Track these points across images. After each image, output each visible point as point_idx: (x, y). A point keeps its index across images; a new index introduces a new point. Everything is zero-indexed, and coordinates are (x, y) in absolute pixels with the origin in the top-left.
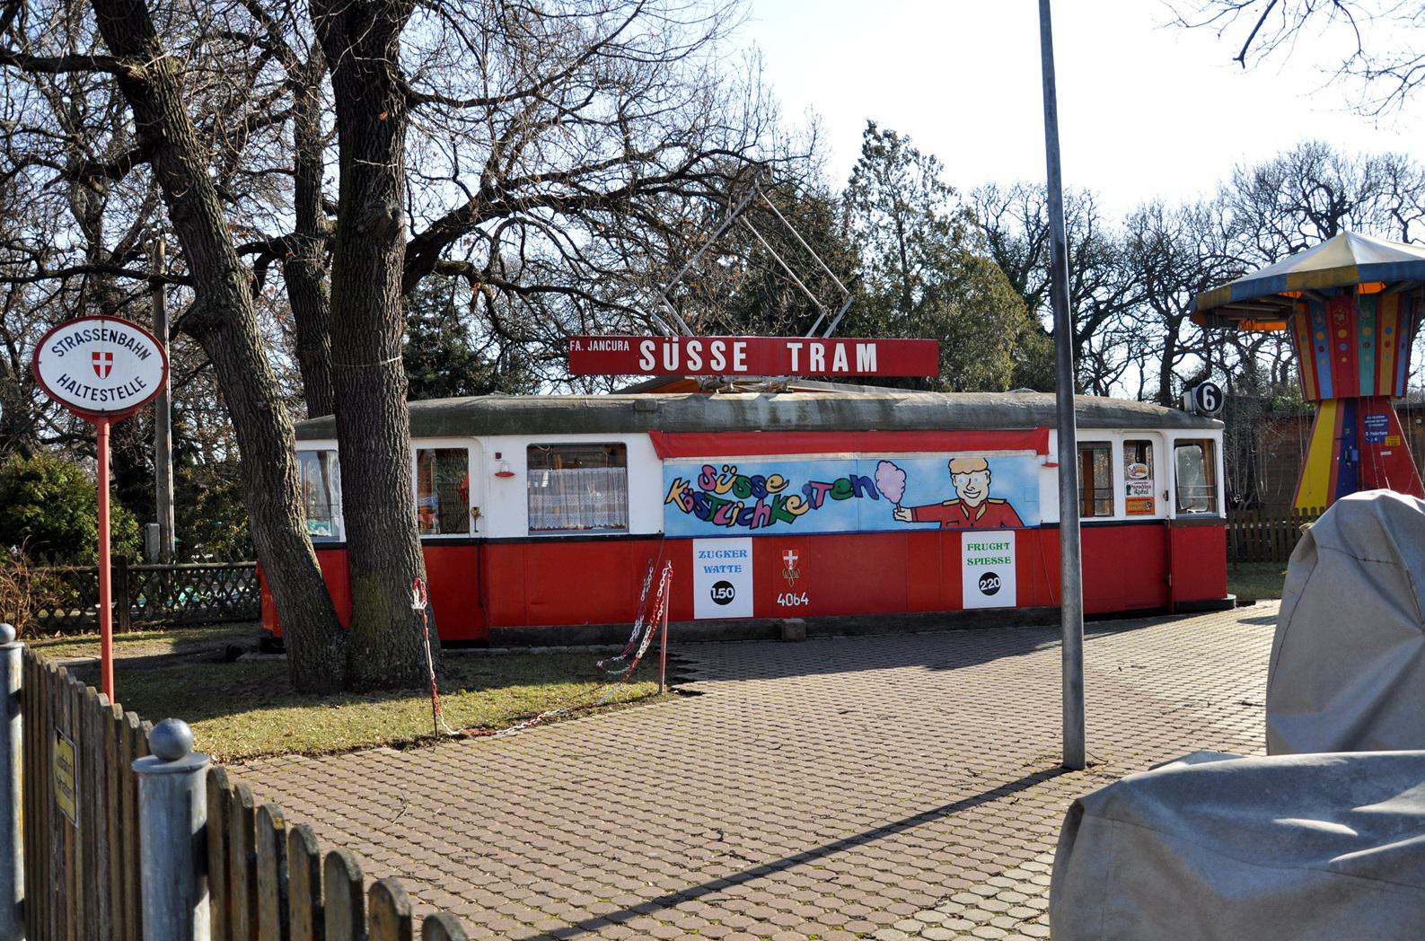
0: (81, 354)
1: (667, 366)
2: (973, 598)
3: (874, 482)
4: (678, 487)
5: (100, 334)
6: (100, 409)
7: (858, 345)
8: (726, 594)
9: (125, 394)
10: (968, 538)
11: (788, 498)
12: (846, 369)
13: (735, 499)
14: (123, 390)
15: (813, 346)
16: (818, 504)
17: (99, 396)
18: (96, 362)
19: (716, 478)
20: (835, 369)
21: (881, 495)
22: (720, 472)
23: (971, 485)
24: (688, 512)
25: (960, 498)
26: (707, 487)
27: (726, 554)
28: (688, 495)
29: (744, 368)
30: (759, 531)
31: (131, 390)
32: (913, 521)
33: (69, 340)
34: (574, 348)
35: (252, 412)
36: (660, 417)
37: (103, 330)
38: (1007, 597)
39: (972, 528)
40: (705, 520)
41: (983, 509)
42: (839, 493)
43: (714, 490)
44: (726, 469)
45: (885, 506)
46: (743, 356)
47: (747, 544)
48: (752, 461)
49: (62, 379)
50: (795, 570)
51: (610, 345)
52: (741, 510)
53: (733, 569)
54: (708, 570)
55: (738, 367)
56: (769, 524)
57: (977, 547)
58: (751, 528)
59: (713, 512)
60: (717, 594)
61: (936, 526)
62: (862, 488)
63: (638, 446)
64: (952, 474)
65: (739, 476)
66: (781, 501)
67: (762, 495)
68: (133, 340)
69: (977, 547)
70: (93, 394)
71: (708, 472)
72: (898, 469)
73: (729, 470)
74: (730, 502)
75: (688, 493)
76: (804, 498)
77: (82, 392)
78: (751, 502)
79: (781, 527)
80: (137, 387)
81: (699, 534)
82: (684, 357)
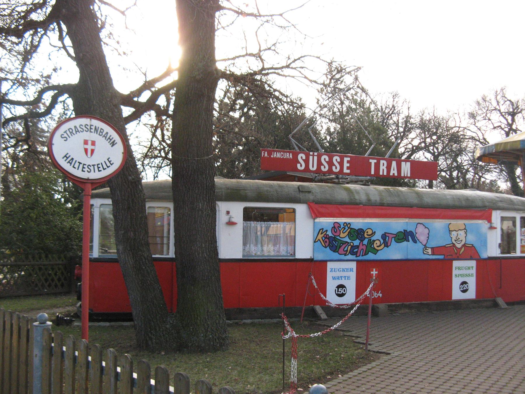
0: (78, 140)
1: (311, 167)
2: (457, 295)
3: (415, 234)
4: (322, 234)
5: (89, 127)
6: (86, 178)
7: (402, 162)
8: (342, 291)
9: (101, 169)
10: (456, 264)
11: (374, 241)
12: (396, 174)
13: (349, 241)
14: (100, 166)
15: (382, 162)
16: (388, 245)
17: (86, 169)
18: (86, 147)
19: (340, 229)
20: (391, 174)
21: (417, 241)
22: (342, 226)
23: (458, 237)
24: (326, 247)
25: (453, 243)
26: (335, 234)
27: (343, 270)
28: (326, 238)
29: (348, 171)
30: (359, 258)
31: (105, 167)
32: (432, 255)
33: (71, 130)
34: (264, 155)
35: (125, 182)
36: (313, 195)
37: (91, 125)
38: (471, 294)
39: (458, 259)
40: (334, 251)
41: (463, 249)
42: (398, 239)
43: (339, 236)
44: (345, 225)
45: (419, 247)
46: (348, 165)
47: (353, 265)
48: (358, 221)
49: (65, 156)
50: (376, 279)
51: (282, 155)
52: (352, 247)
53: (346, 278)
54: (334, 278)
55: (346, 171)
56: (365, 254)
57: (459, 268)
58: (356, 257)
59: (338, 248)
60: (338, 291)
61: (441, 257)
62: (409, 237)
63: (301, 210)
64: (450, 231)
65: (351, 229)
66: (371, 242)
67: (362, 239)
68: (107, 133)
69: (459, 268)
70: (83, 168)
71: (336, 226)
72: (426, 227)
73: (347, 225)
74: (347, 242)
75: (326, 237)
76: (382, 241)
77: (77, 165)
78: (357, 242)
79: (371, 256)
80: (109, 164)
81: (330, 259)
82: (320, 164)
